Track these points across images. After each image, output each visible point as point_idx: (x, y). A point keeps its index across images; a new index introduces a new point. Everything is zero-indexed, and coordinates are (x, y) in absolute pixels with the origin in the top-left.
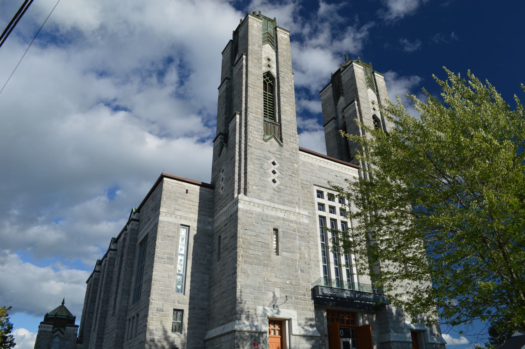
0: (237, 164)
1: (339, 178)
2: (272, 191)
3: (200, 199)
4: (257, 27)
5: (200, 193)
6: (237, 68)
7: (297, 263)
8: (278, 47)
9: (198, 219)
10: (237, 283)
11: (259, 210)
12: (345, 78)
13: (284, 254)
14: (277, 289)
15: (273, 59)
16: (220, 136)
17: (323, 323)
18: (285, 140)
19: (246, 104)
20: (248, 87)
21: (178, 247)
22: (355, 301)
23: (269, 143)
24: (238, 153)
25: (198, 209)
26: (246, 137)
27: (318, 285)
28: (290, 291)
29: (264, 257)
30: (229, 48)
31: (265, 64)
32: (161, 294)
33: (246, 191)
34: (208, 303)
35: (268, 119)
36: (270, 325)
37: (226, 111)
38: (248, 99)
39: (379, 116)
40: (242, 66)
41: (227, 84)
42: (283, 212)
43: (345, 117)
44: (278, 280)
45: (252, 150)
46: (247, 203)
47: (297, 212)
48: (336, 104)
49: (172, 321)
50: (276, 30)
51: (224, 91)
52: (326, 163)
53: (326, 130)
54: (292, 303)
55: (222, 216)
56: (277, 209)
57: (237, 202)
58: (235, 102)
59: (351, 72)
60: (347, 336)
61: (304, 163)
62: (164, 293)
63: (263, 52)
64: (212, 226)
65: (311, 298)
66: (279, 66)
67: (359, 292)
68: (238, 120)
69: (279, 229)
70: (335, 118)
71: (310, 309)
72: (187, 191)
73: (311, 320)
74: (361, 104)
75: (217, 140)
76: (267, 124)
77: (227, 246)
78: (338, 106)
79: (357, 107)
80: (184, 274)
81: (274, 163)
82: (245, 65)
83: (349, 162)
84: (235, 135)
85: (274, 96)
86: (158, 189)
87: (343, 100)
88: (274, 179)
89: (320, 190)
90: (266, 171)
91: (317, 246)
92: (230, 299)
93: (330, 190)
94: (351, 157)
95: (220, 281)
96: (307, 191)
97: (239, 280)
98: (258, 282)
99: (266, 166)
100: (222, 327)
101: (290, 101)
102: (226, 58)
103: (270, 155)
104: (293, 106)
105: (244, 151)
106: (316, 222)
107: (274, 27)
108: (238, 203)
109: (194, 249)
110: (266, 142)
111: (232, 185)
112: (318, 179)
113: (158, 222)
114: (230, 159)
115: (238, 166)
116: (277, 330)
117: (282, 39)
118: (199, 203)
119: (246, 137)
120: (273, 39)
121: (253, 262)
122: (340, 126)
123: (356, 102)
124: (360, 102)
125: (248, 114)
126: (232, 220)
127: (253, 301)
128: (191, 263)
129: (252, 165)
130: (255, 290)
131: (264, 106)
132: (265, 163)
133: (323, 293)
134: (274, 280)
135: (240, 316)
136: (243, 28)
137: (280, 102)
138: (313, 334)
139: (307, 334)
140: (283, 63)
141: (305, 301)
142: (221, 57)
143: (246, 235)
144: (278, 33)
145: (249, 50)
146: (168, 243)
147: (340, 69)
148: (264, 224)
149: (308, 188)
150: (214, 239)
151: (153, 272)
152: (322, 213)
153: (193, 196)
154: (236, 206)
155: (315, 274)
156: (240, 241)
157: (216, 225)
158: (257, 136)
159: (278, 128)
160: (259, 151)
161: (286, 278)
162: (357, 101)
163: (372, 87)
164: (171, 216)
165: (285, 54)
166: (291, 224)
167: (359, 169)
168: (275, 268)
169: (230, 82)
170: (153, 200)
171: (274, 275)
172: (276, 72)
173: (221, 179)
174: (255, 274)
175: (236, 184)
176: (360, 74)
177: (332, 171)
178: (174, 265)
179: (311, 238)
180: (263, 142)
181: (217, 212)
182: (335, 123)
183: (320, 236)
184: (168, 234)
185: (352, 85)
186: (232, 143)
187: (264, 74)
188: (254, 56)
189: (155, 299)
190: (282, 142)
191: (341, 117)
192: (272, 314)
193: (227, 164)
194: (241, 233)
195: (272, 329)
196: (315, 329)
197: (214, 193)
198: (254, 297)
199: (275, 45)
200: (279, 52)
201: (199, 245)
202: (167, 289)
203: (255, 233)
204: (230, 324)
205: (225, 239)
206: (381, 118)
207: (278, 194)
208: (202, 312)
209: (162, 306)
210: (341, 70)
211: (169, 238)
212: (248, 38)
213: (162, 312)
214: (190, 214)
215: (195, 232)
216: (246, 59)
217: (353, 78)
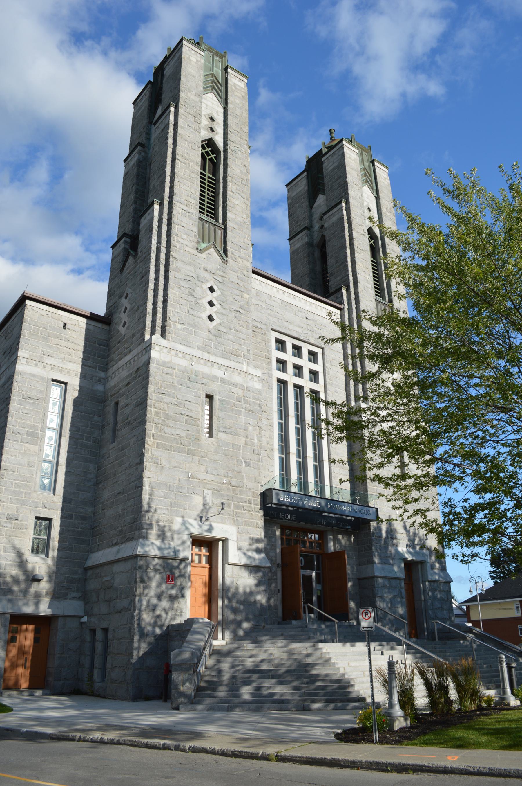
0: (151, 286)
1: (310, 322)
2: (207, 333)
3: (87, 340)
4: (196, 63)
5: (87, 330)
6: (158, 127)
7: (241, 451)
8: (229, 101)
9: (81, 373)
10: (144, 479)
11: (184, 363)
12: (328, 165)
13: (221, 436)
14: (208, 490)
15: (220, 118)
16: (124, 239)
17: (274, 547)
18: (232, 253)
19: (172, 188)
20: (177, 161)
21: (47, 416)
22: (323, 514)
23: (206, 255)
24: (154, 267)
25: (82, 356)
26: (169, 242)
27: (273, 487)
28: (227, 495)
29: (190, 439)
30: (145, 94)
31: (205, 125)
32: (15, 492)
33: (165, 330)
34: (93, 509)
35: (205, 216)
36: (194, 547)
37: (136, 198)
38: (176, 179)
39: (377, 231)
40: (168, 124)
41: (139, 153)
42: (222, 369)
43: (325, 227)
44: (210, 477)
45: (178, 265)
46: (165, 350)
47: (245, 370)
48: (311, 207)
49: (32, 536)
50: (226, 72)
51: (134, 164)
52: (292, 296)
53: (292, 245)
54: (229, 514)
55: (123, 370)
56: (213, 363)
57: (149, 347)
58: (153, 184)
59: (340, 157)
60: (309, 566)
61: (258, 294)
62: (21, 490)
63: (204, 106)
64: (105, 384)
65: (259, 507)
66: (229, 132)
67: (331, 500)
68: (156, 213)
69: (214, 397)
70: (309, 228)
71: (257, 524)
72: (65, 324)
73: (258, 541)
74: (351, 208)
75: (119, 244)
76: (203, 225)
77: (129, 419)
78: (313, 210)
79: (345, 213)
80: (55, 461)
81: (212, 289)
82: (173, 123)
83: (327, 298)
84: (151, 237)
85: (217, 181)
86: (15, 319)
87: (322, 200)
88: (211, 315)
89: (281, 338)
90: (198, 301)
91: (272, 426)
92: (131, 505)
93: (296, 340)
94: (331, 292)
95: (115, 475)
96: (260, 338)
97: (146, 474)
98: (178, 479)
99: (198, 292)
100: (115, 548)
101: (243, 191)
102: (140, 112)
103: (206, 275)
104: (248, 200)
105: (164, 265)
106: (272, 389)
107: (224, 67)
108: (151, 349)
109: (72, 421)
110: (201, 253)
111: (142, 320)
112: (278, 321)
113: (14, 372)
114: (139, 277)
115: (153, 288)
116: (204, 555)
117: (236, 88)
118: (85, 346)
119: (169, 242)
120: (220, 86)
121: (171, 446)
122: (315, 242)
123: (344, 205)
124: (351, 206)
125: (173, 205)
126: (139, 377)
127: (168, 509)
128: (68, 443)
129: (176, 289)
130: (173, 491)
131: (201, 195)
132: (198, 288)
133: (279, 500)
134: (203, 476)
135: (147, 533)
136: (172, 63)
137: (227, 191)
138: (260, 563)
139: (251, 562)
140: (234, 127)
141: (249, 511)
142: (131, 109)
143: (161, 402)
144: (229, 78)
145: (180, 99)
146: (29, 410)
147: (321, 150)
148: (191, 386)
149: (262, 333)
150: (107, 406)
151: (2, 455)
152: (283, 376)
153: (74, 335)
154: (147, 353)
155: (267, 470)
156: (151, 412)
157: (112, 383)
158: (186, 242)
159: (221, 233)
160: (188, 267)
161: (222, 474)
162: (346, 204)
163: (369, 184)
164: (36, 364)
165: (238, 114)
166: (234, 390)
167: (342, 311)
168: (206, 458)
169: (145, 152)
170: (6, 337)
171: (203, 468)
172: (222, 140)
173: (123, 309)
174: (174, 466)
175: (149, 318)
176: (354, 160)
177: (300, 310)
178: (38, 446)
179: (264, 413)
180: (196, 252)
181: (113, 363)
182: (307, 236)
183: (277, 410)
184: (30, 395)
185: (340, 177)
186: (144, 251)
187: (202, 141)
188: (188, 110)
189: (4, 500)
190: (226, 256)
191: (317, 227)
192: (200, 531)
193: (133, 285)
194: (153, 399)
195: (196, 554)
196: (263, 555)
197: (110, 331)
198: (171, 503)
199: (224, 97)
200: (229, 108)
201: (81, 415)
202: (26, 485)
203: (176, 399)
204: (129, 544)
205: (126, 406)
206: (381, 234)
207: (216, 339)
208: (82, 524)
209: (17, 511)
210: (324, 152)
211: (32, 401)
212: (180, 79)
213: (16, 522)
214: (69, 364)
215: (76, 394)
216: (175, 113)
217: (342, 166)
